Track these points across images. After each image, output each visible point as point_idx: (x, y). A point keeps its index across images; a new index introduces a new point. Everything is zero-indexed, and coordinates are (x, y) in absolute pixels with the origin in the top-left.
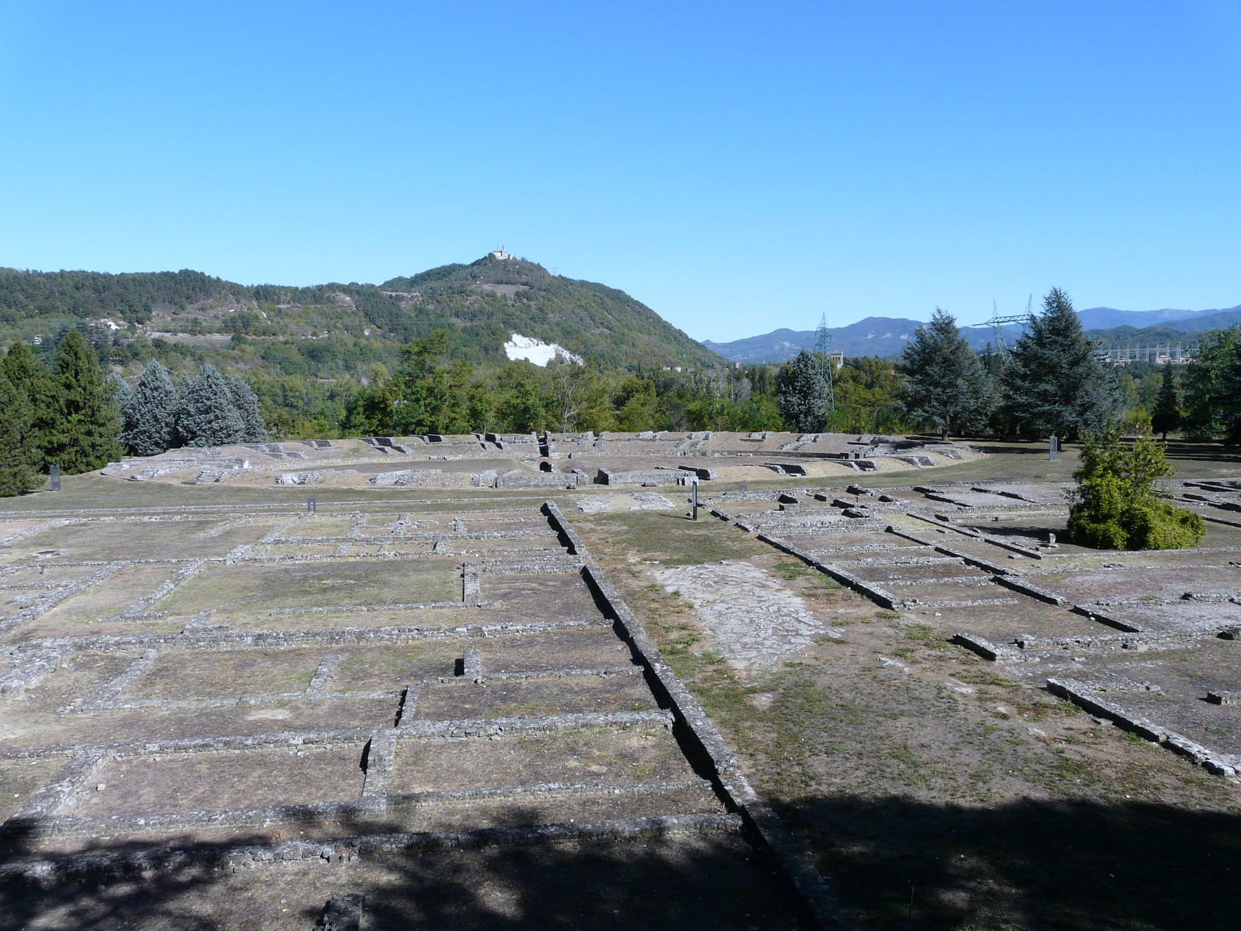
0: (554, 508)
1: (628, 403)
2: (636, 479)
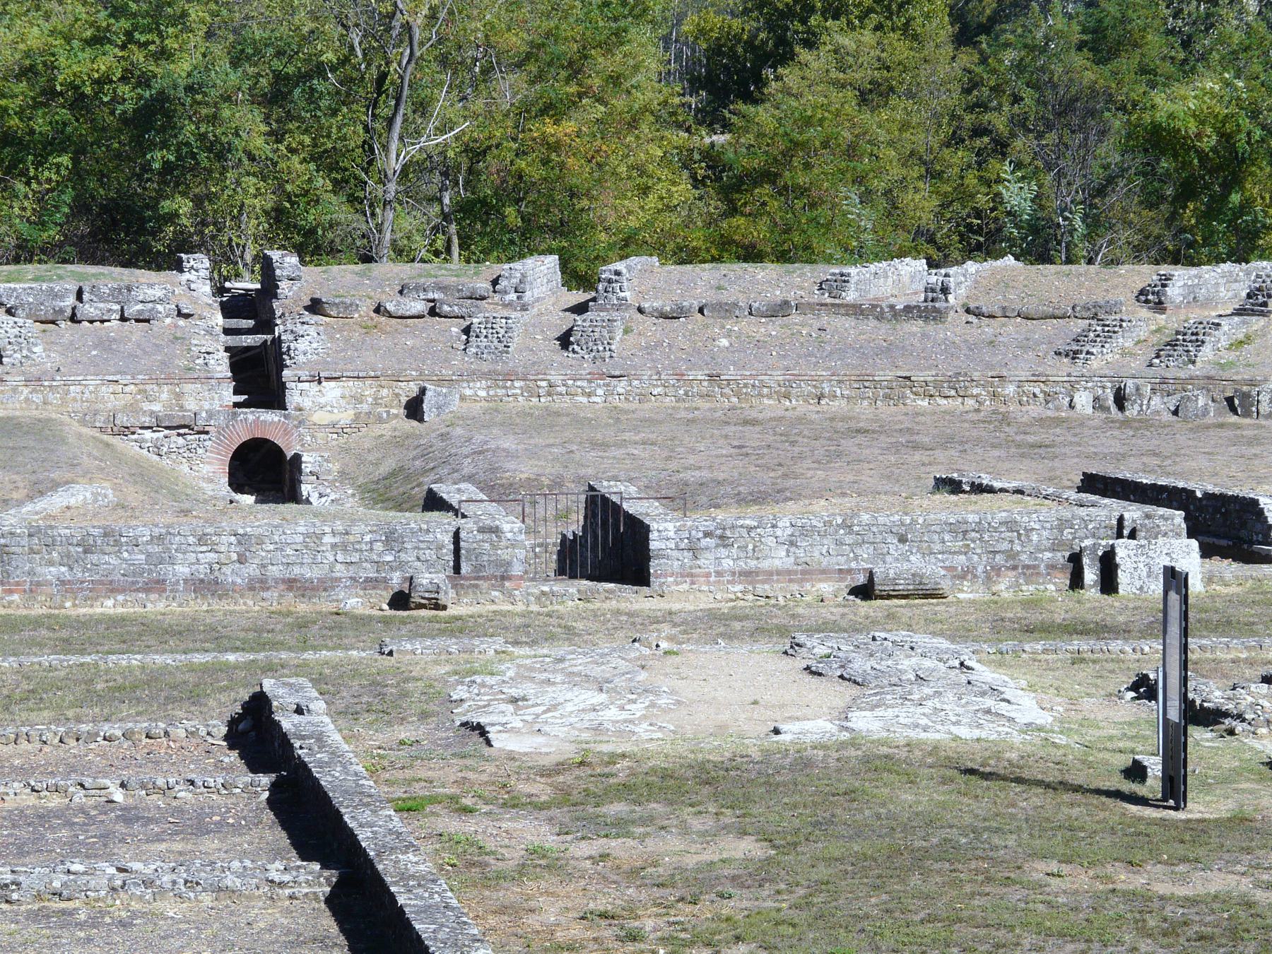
0: (318, 730)
1: (786, 80)
2: (818, 552)
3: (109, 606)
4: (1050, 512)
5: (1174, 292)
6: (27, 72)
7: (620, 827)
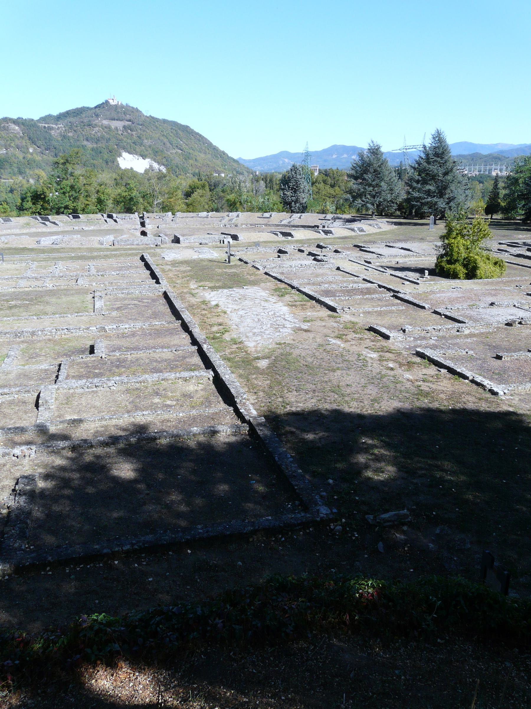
2: (196, 240)
3: (128, 247)
4: (218, 236)
5: (230, 215)
6: (119, 195)
7: (177, 266)
